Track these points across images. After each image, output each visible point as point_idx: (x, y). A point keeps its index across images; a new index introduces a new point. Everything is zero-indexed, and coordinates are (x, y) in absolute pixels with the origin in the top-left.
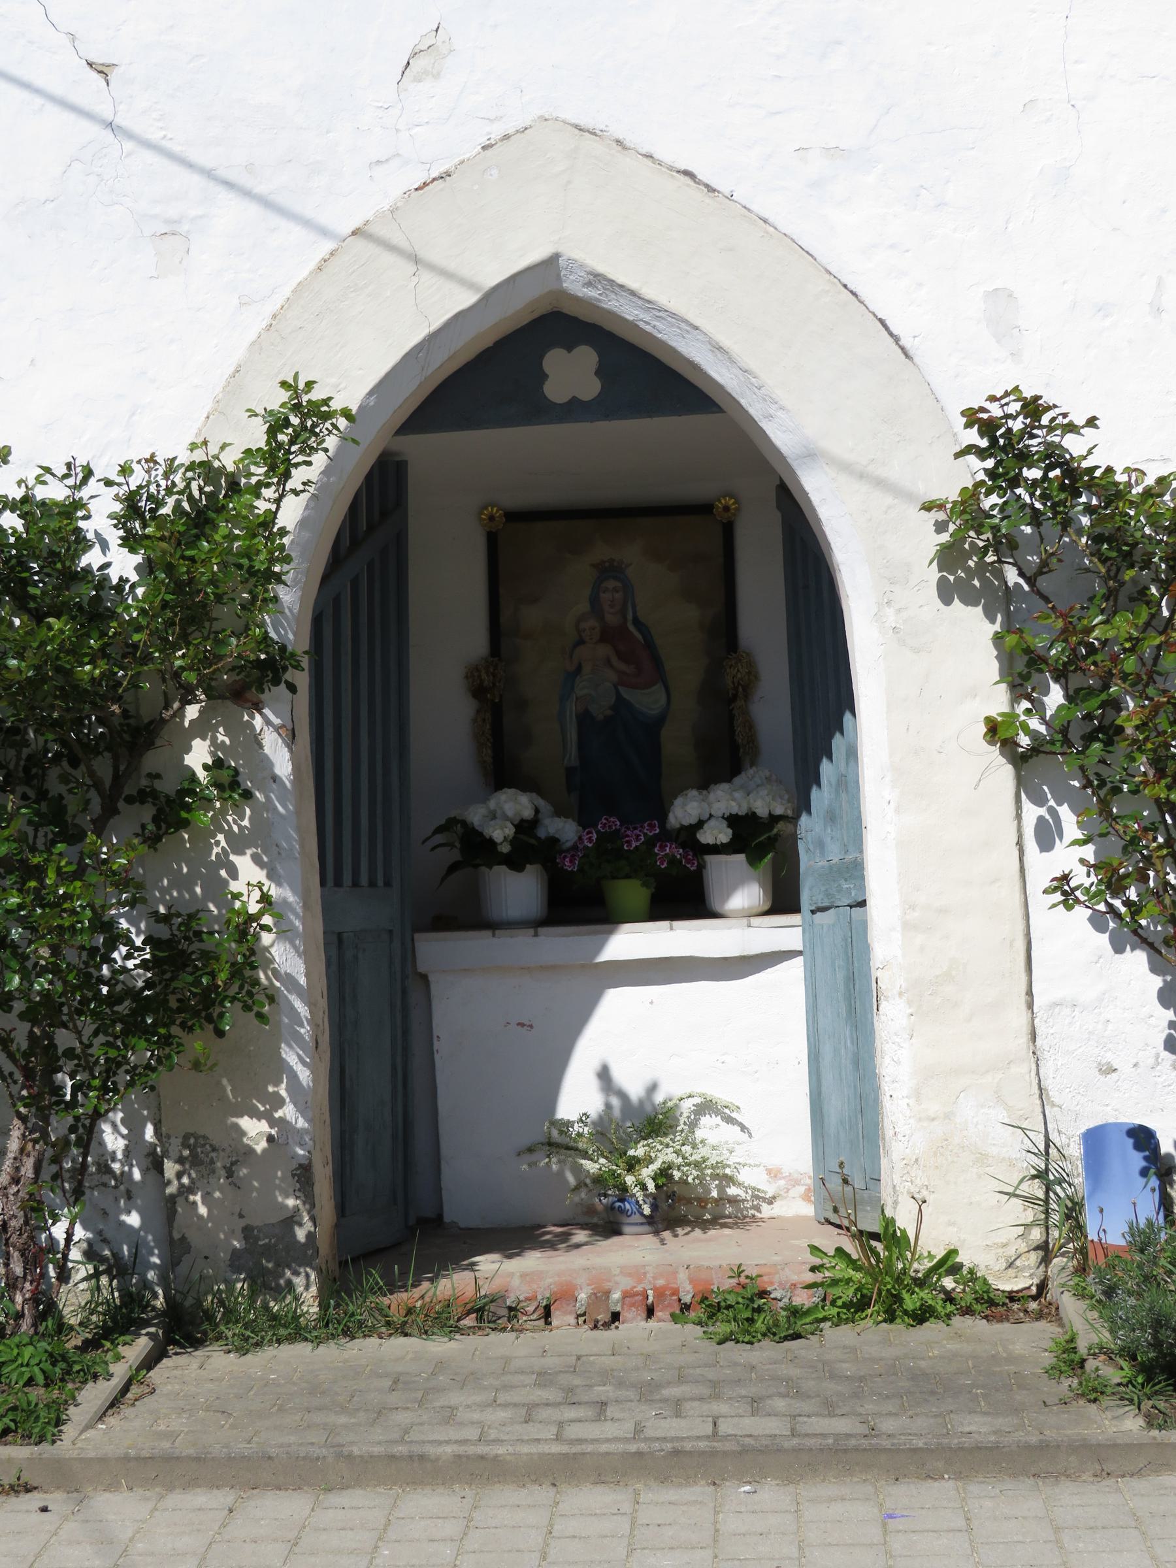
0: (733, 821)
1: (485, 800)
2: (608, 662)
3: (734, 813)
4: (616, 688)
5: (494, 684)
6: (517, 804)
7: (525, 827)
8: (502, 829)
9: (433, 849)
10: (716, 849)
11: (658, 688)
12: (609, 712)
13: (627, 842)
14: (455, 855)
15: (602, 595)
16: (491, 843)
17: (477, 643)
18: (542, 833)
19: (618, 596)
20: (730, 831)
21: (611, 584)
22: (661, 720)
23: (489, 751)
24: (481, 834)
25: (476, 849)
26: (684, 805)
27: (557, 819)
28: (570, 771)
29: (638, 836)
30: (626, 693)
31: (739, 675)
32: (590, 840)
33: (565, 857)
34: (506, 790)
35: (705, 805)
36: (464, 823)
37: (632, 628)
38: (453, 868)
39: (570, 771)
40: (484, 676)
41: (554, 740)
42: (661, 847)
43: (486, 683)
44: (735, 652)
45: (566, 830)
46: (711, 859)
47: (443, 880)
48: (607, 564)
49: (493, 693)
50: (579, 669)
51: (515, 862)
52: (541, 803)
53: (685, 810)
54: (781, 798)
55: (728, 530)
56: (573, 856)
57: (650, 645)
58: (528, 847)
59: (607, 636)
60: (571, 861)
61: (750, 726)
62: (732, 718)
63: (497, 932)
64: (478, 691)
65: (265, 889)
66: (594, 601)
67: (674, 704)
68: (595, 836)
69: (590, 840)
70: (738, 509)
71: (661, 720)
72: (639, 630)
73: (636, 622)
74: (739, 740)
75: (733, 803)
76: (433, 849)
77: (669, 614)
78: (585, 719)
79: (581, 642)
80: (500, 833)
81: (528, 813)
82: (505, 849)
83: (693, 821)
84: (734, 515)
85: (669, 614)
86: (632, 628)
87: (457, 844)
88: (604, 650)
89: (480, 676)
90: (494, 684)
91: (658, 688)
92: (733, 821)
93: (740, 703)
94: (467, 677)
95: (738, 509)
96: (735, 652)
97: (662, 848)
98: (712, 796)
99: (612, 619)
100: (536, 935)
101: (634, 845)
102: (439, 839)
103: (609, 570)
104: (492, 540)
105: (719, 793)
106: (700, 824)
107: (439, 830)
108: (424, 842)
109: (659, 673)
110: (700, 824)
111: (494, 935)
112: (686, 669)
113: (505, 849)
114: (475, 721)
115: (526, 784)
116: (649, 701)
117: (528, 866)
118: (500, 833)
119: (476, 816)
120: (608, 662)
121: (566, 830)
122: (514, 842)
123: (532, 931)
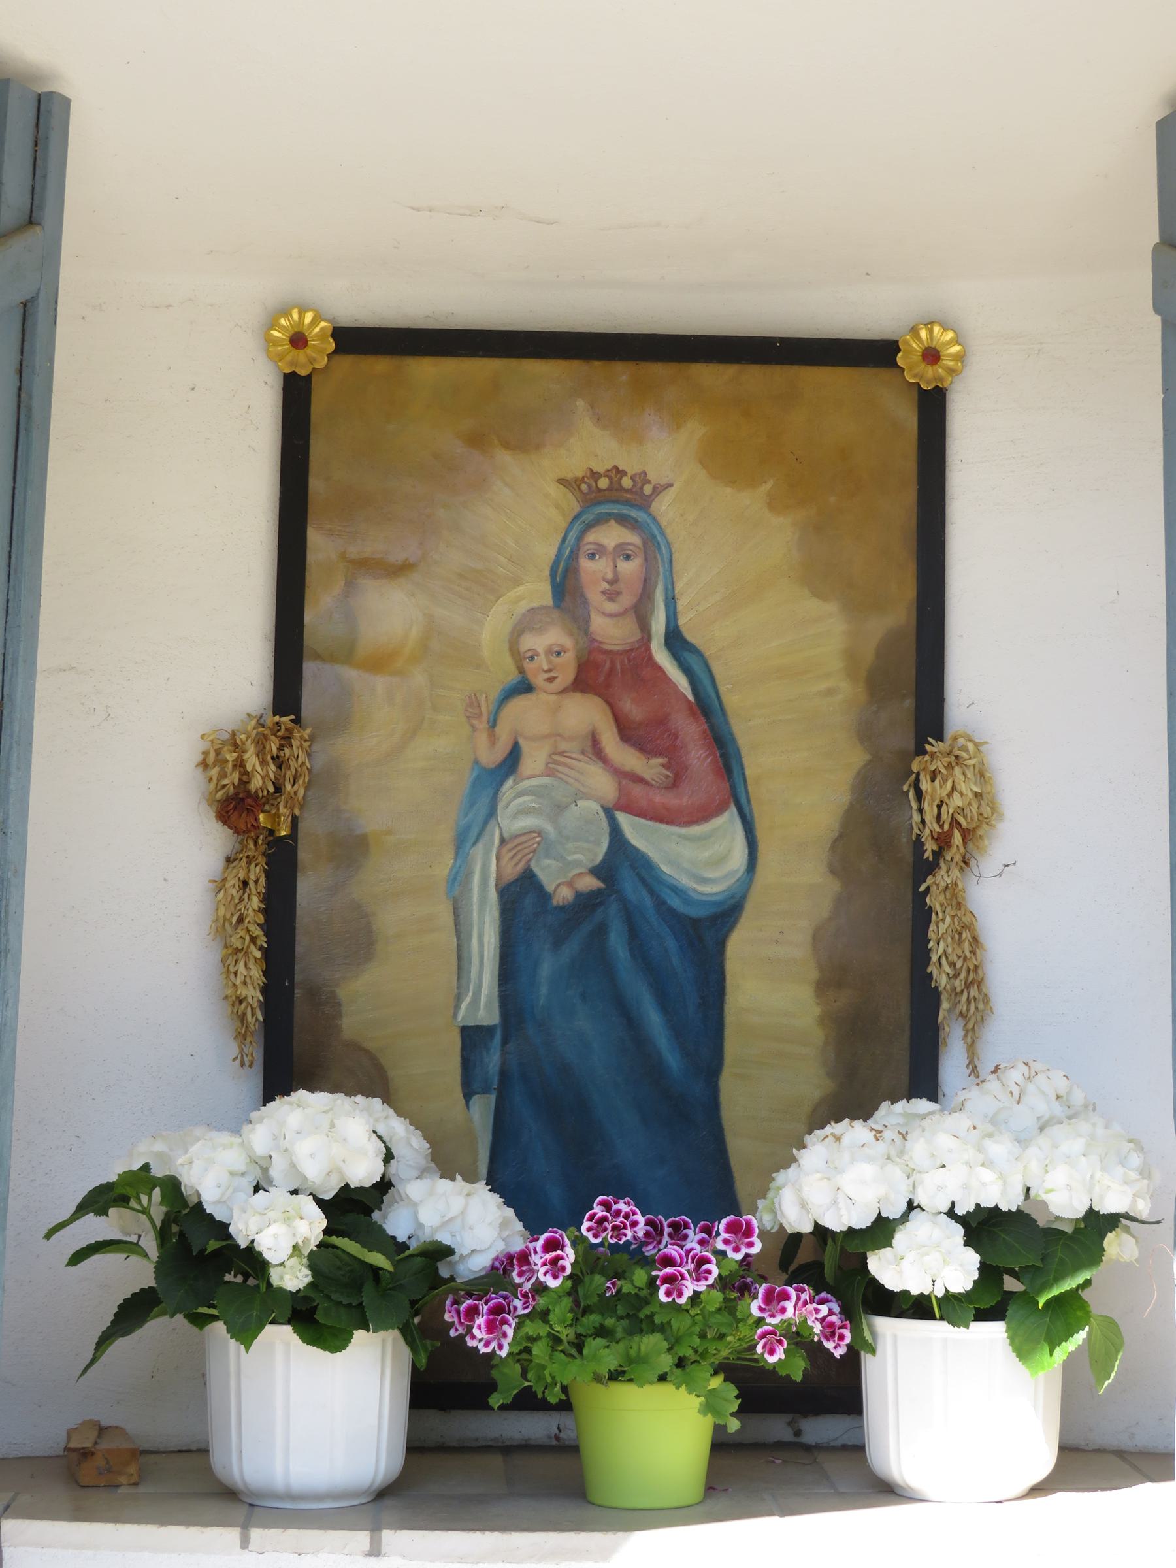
0: (982, 1227)
1: (237, 1125)
2: (596, 749)
3: (987, 1203)
4: (609, 813)
5: (278, 789)
6: (332, 1137)
7: (351, 1209)
8: (287, 1221)
9: (78, 1257)
10: (918, 1308)
11: (728, 822)
12: (590, 883)
13: (670, 1279)
14: (139, 1274)
15: (585, 564)
16: (252, 1261)
17: (239, 678)
18: (397, 1223)
19: (630, 568)
20: (972, 1259)
21: (611, 536)
22: (727, 914)
23: (256, 973)
24: (222, 1229)
25: (202, 1269)
26: (832, 1169)
27: (445, 1185)
28: (473, 1037)
29: (702, 1261)
30: (634, 830)
31: (957, 801)
32: (555, 1266)
33: (472, 1312)
34: (301, 1095)
35: (896, 1172)
36: (172, 1186)
37: (662, 657)
38: (134, 1312)
39: (473, 1037)
40: (252, 761)
41: (428, 955)
42: (769, 1298)
43: (256, 783)
44: (940, 737)
45: (469, 1221)
46: (887, 1328)
47: (105, 1340)
48: (603, 483)
49: (270, 821)
50: (512, 761)
51: (322, 1315)
52: (398, 1128)
53: (829, 1182)
54: (1123, 1162)
55: (932, 408)
56: (497, 1310)
57: (707, 708)
58: (364, 1274)
59: (593, 675)
60: (491, 1327)
61: (969, 935)
62: (922, 916)
63: (256, 1534)
64: (236, 807)
65: (246, 757)
66: (565, 584)
67: (769, 873)
68: (569, 1255)
69: (555, 1266)
70: (960, 357)
71: (727, 914)
72: (687, 671)
73: (675, 640)
74: (941, 980)
75: (987, 1175)
76: (78, 1257)
77: (767, 626)
78: (520, 896)
79: (524, 687)
80: (283, 1236)
81: (363, 1171)
82: (292, 1277)
83: (861, 1220)
84: (952, 371)
85: (767, 626)
86: (662, 657)
87: (150, 1244)
88: (585, 713)
89: (240, 764)
90: (278, 789)
91: (728, 822)
92: (982, 1227)
93: (943, 876)
94: (204, 765)
95: (960, 357)
96: (940, 737)
97: (774, 1300)
98: (918, 1149)
99: (611, 629)
100: (375, 1551)
101: (689, 1287)
102: (95, 1227)
103: (611, 498)
104: (296, 394)
105: (944, 1141)
106: (882, 1231)
107: (100, 1200)
108: (49, 1235)
109: (730, 785)
110: (882, 1231)
111: (245, 1543)
112: (803, 776)
113: (292, 1277)
114: (220, 885)
115: (365, 1077)
116: (696, 858)
117: (359, 1335)
118: (283, 1236)
119: (211, 1173)
120: (596, 749)
121: (469, 1221)
122: (321, 1259)
123: (363, 1538)
